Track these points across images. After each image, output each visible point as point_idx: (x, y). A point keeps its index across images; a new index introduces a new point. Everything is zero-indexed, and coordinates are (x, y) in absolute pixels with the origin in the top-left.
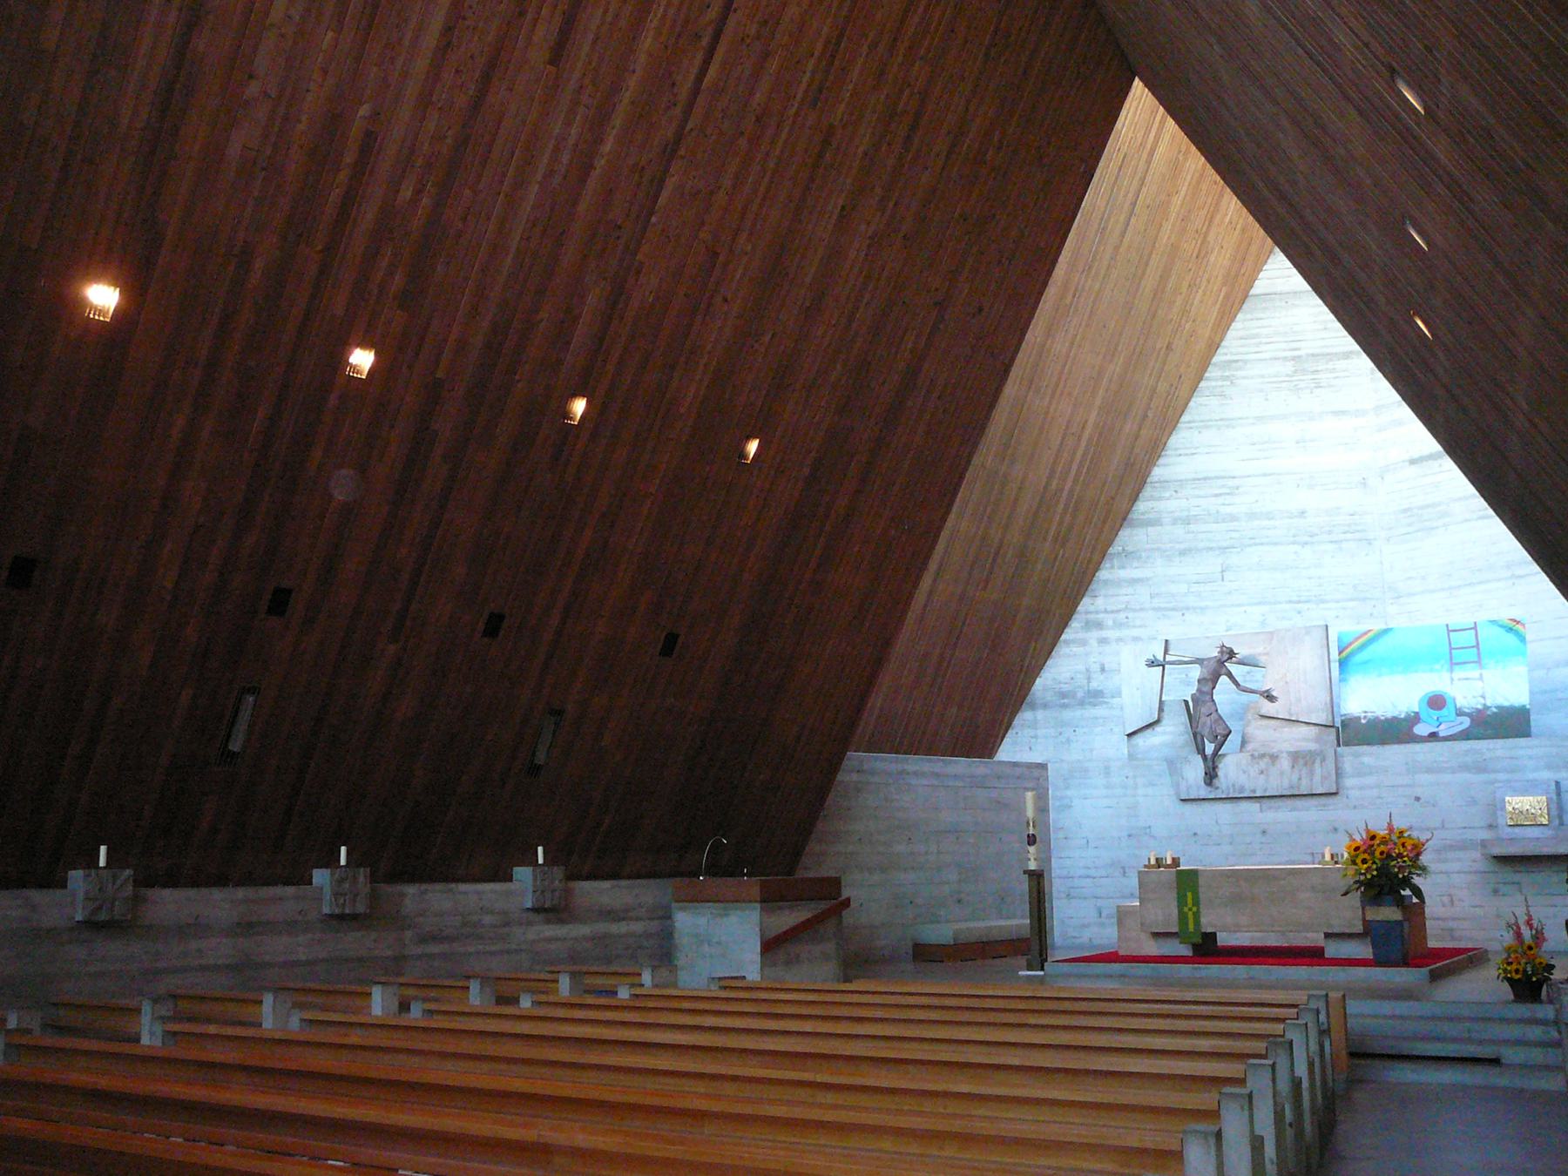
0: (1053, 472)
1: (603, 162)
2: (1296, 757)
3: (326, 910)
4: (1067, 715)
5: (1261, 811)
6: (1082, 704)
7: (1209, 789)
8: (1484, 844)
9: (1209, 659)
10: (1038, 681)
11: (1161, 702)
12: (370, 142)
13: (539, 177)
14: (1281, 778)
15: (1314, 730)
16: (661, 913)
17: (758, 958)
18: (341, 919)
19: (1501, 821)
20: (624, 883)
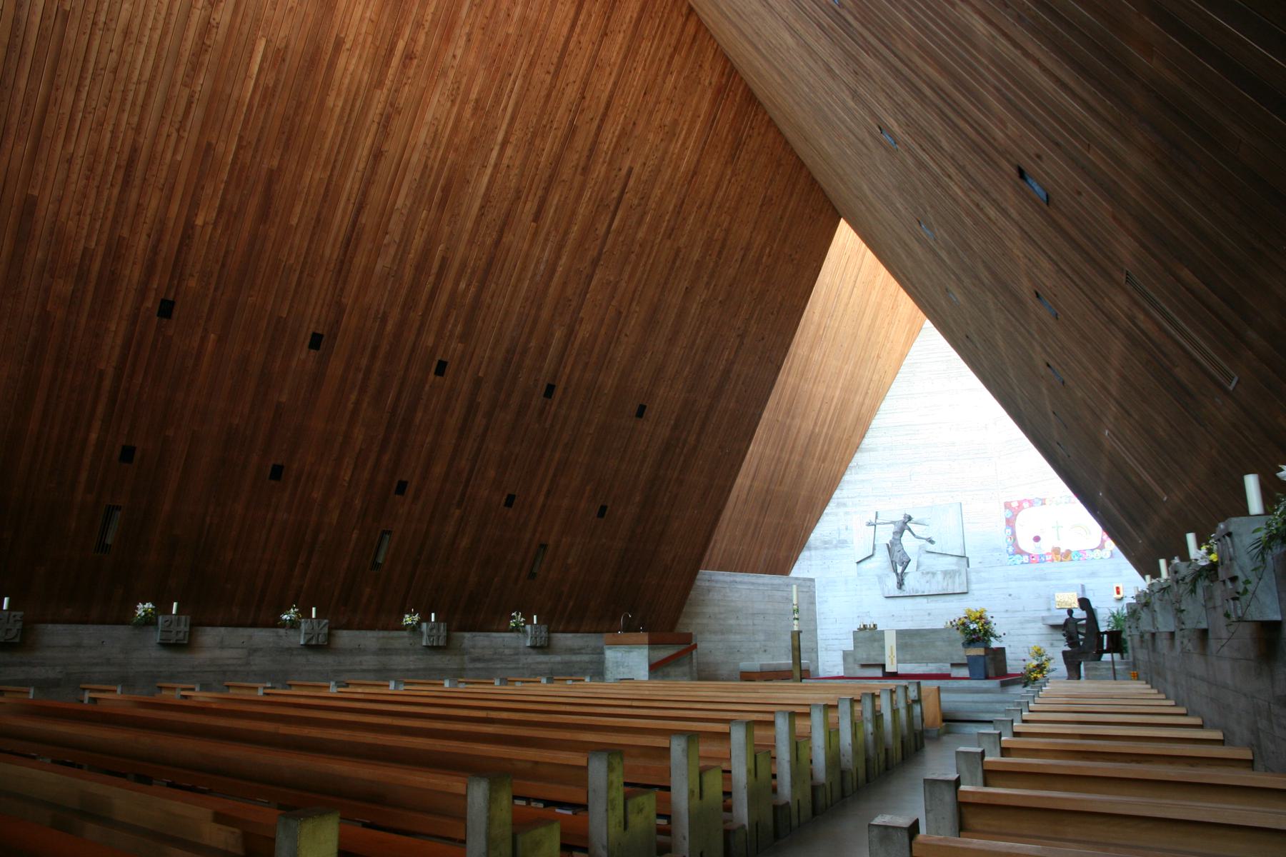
0: (816, 424)
1: (561, 269)
2: (945, 573)
3: (424, 644)
4: (828, 553)
5: (928, 603)
6: (836, 547)
7: (900, 591)
8: (1043, 619)
9: (898, 522)
10: (812, 535)
11: (874, 546)
12: (444, 262)
13: (529, 277)
14: (937, 585)
15: (955, 559)
16: (598, 651)
17: (647, 674)
18: (432, 649)
19: (1053, 607)
20: (579, 635)
